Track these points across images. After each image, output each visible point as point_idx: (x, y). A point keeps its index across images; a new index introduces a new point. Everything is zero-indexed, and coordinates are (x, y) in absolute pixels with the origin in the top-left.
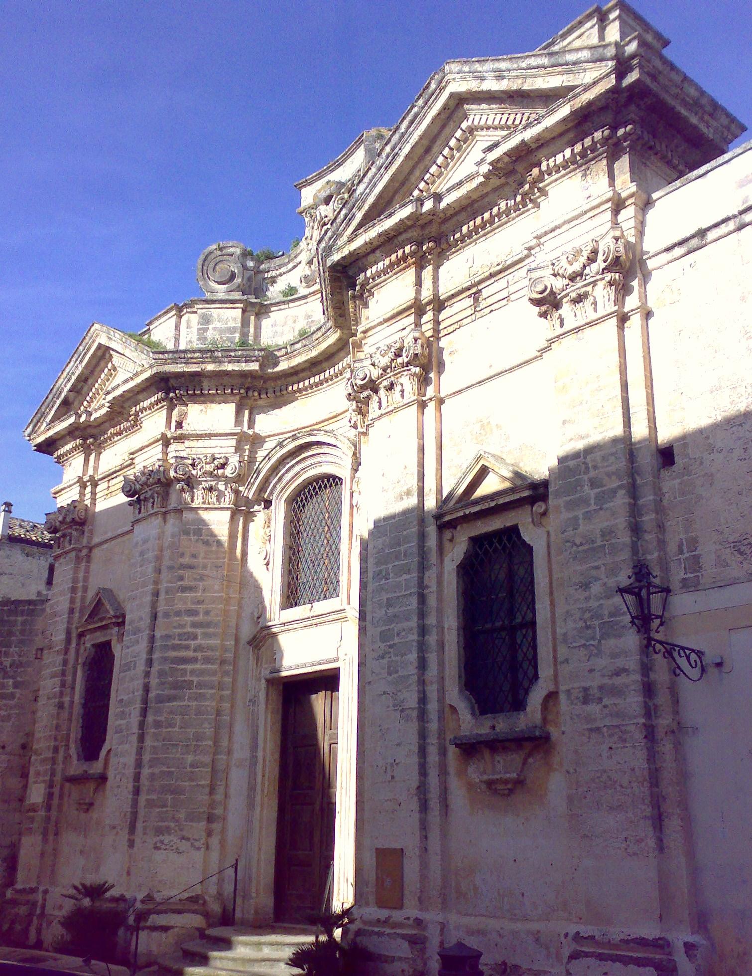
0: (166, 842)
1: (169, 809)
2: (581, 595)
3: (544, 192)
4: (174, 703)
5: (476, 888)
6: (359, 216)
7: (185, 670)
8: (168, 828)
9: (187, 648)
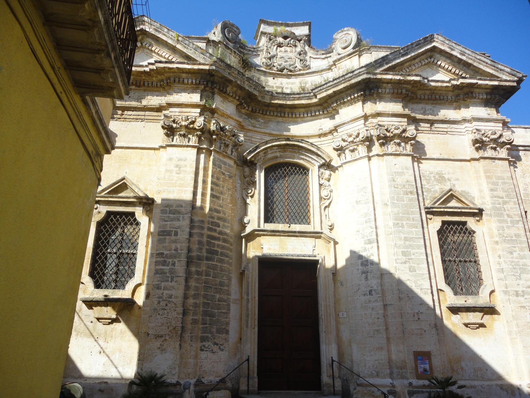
0: (206, 346)
1: (208, 325)
2: (509, 256)
3: (338, 113)
4: (210, 262)
5: (462, 369)
6: (386, 67)
7: (214, 244)
8: (207, 337)
9: (215, 231)
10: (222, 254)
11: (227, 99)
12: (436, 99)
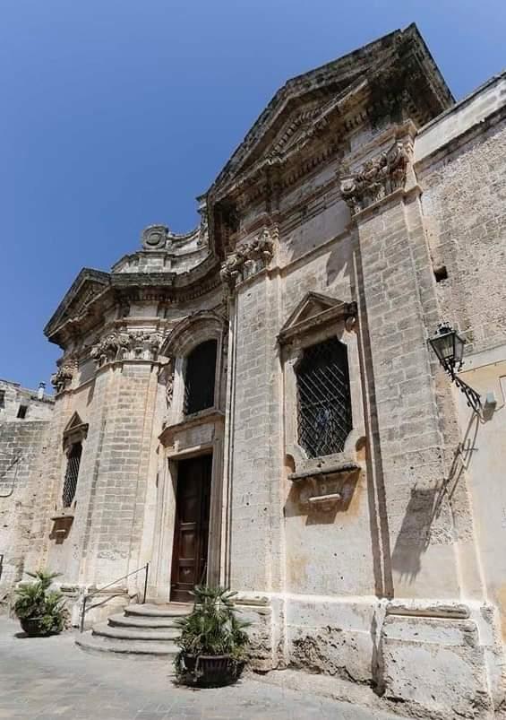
10: (129, 462)
11: (144, 304)
12: (309, 170)
